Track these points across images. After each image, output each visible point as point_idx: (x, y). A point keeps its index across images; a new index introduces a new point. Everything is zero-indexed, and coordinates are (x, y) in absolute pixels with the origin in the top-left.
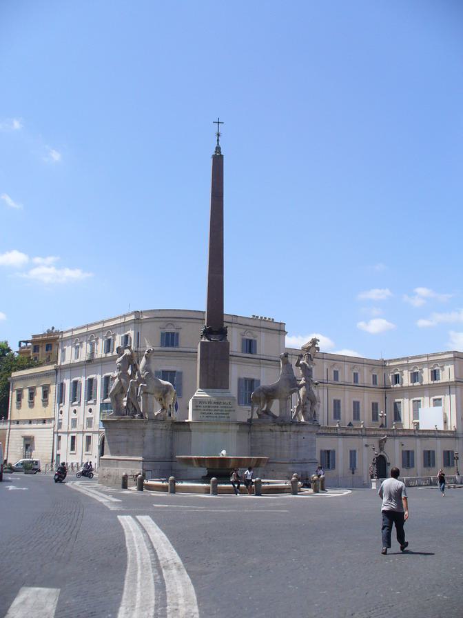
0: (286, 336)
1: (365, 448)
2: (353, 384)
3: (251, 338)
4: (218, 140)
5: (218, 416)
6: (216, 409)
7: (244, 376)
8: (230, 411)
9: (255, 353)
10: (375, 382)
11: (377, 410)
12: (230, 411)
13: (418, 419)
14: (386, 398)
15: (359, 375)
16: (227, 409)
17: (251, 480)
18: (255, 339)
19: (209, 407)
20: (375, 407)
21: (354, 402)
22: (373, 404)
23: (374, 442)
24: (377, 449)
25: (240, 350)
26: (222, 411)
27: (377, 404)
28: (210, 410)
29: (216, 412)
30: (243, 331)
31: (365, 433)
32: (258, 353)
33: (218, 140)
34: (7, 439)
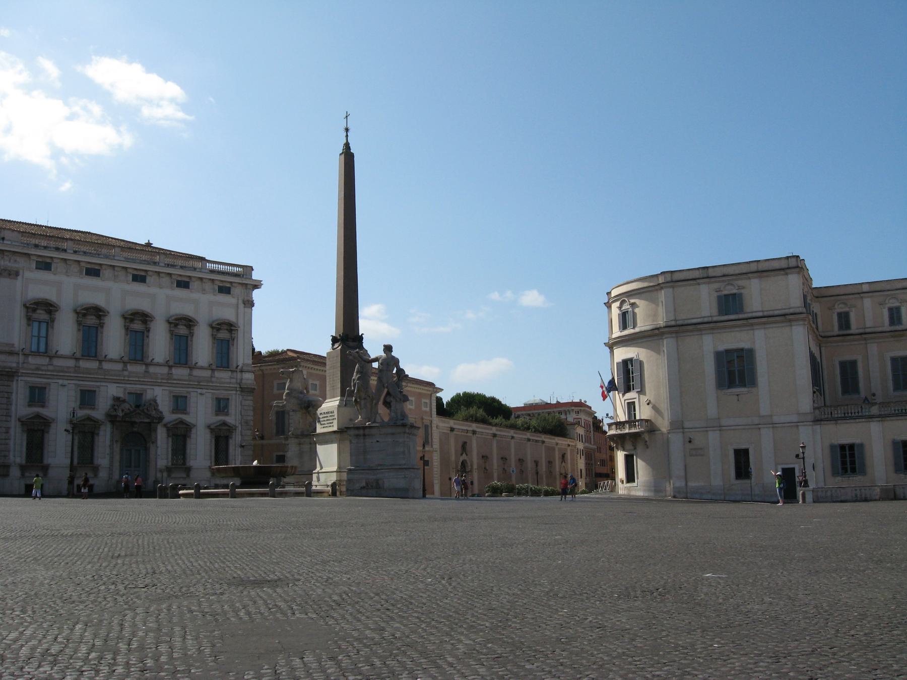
3: (735, 291)
4: (347, 136)
5: (328, 425)
7: (721, 348)
33: (347, 136)
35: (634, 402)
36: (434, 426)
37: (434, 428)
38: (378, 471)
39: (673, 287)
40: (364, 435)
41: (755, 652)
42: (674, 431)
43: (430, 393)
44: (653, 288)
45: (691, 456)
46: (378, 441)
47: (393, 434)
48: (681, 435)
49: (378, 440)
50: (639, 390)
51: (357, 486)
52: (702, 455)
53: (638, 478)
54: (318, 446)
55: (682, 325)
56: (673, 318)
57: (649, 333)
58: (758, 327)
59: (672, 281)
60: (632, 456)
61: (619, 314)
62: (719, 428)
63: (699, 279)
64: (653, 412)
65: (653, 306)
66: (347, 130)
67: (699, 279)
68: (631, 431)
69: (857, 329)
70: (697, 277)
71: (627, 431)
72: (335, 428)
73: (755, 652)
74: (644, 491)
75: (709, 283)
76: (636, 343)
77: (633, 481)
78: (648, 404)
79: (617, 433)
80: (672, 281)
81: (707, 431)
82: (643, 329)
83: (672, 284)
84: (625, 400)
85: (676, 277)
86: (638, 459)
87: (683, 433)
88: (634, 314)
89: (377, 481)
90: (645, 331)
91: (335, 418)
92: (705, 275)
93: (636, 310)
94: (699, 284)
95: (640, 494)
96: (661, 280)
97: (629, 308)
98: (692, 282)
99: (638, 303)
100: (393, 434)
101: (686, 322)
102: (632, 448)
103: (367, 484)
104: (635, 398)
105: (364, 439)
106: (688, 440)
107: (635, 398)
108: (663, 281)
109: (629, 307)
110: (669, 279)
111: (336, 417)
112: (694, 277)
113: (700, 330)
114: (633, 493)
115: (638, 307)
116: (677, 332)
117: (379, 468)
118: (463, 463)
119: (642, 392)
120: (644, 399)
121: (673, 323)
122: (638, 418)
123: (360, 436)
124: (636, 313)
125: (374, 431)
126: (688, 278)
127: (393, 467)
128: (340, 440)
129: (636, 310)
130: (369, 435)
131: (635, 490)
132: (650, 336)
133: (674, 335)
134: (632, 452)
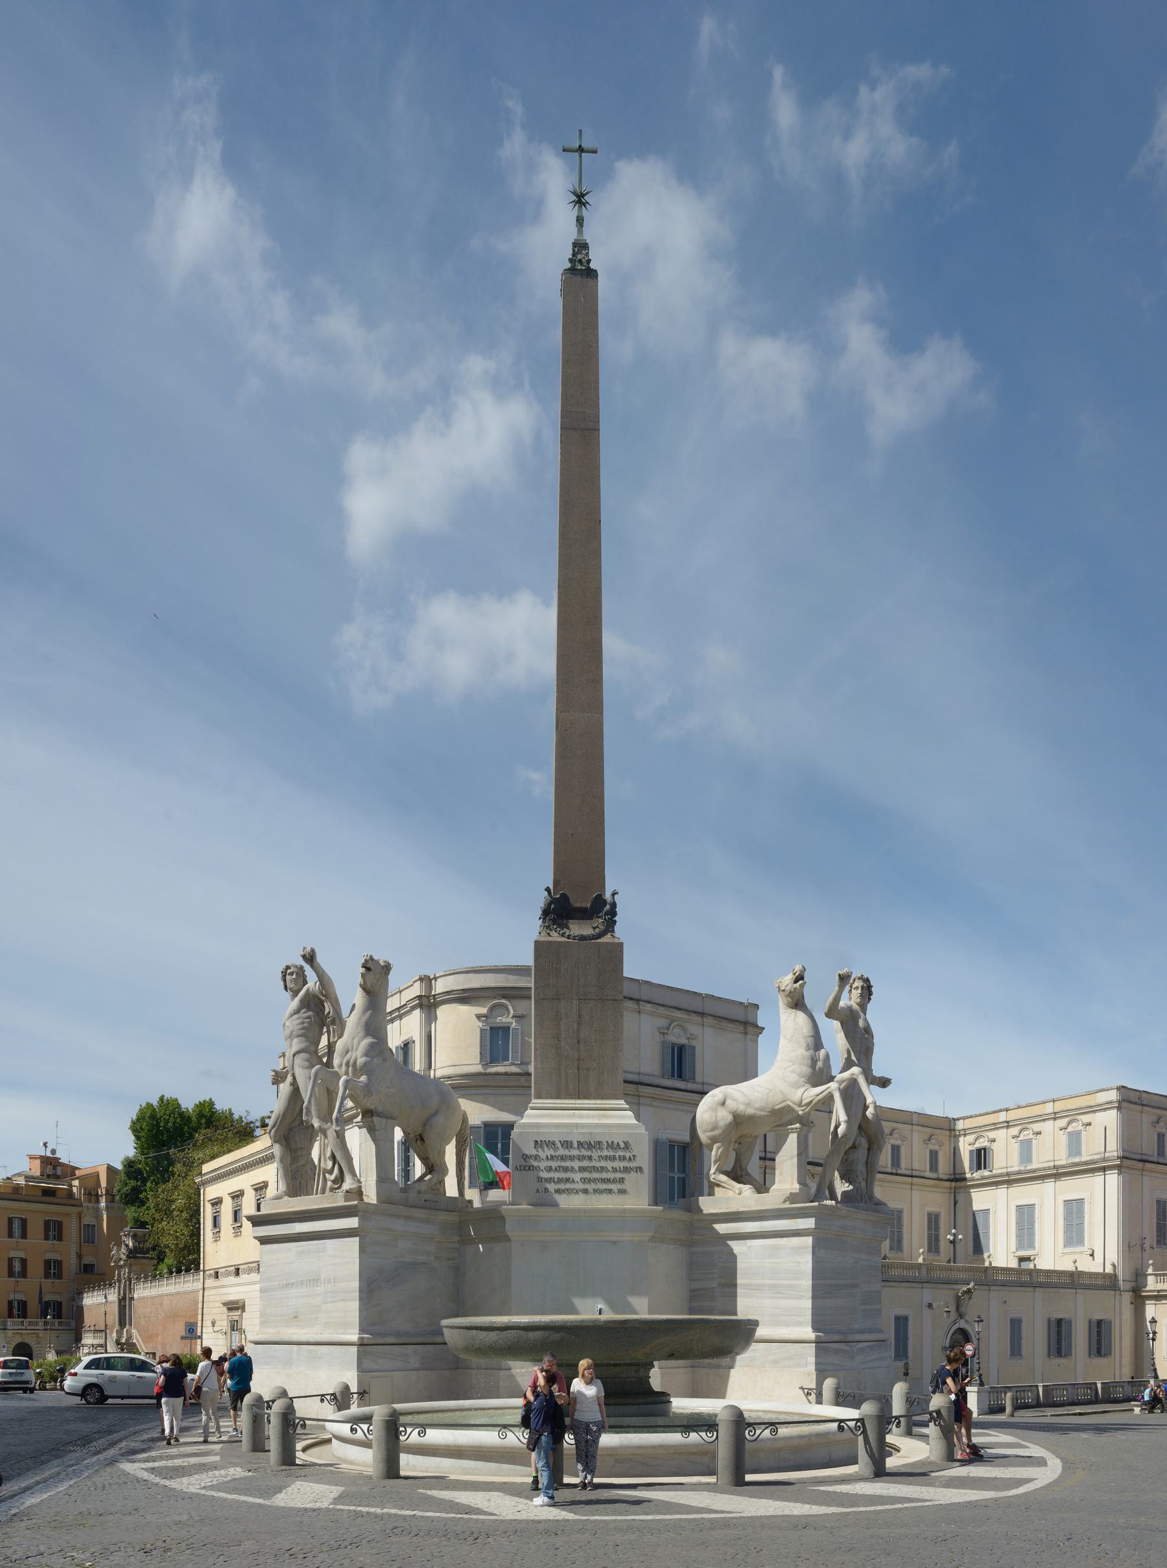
0: (761, 1038)
1: (926, 1311)
2: (889, 1170)
3: (683, 1041)
5: (591, 1187)
6: (585, 1163)
8: (626, 1170)
9: (693, 1079)
10: (934, 1166)
11: (937, 1228)
12: (626, 1170)
13: (1031, 1246)
14: (955, 1203)
15: (903, 1150)
16: (617, 1164)
17: (54, 1318)
18: (694, 1043)
19: (563, 1158)
20: (933, 1221)
21: (929, 1215)
22: (929, 1215)
23: (943, 1298)
24: (954, 1315)
25: (657, 1072)
26: (603, 1169)
27: (937, 1216)
28: (566, 1169)
29: (586, 1175)
30: (663, 1022)
31: (925, 1278)
32: (698, 1078)
33: (580, 221)
34: (200, 1311)
69: (905, 1169)
91: (639, 1169)
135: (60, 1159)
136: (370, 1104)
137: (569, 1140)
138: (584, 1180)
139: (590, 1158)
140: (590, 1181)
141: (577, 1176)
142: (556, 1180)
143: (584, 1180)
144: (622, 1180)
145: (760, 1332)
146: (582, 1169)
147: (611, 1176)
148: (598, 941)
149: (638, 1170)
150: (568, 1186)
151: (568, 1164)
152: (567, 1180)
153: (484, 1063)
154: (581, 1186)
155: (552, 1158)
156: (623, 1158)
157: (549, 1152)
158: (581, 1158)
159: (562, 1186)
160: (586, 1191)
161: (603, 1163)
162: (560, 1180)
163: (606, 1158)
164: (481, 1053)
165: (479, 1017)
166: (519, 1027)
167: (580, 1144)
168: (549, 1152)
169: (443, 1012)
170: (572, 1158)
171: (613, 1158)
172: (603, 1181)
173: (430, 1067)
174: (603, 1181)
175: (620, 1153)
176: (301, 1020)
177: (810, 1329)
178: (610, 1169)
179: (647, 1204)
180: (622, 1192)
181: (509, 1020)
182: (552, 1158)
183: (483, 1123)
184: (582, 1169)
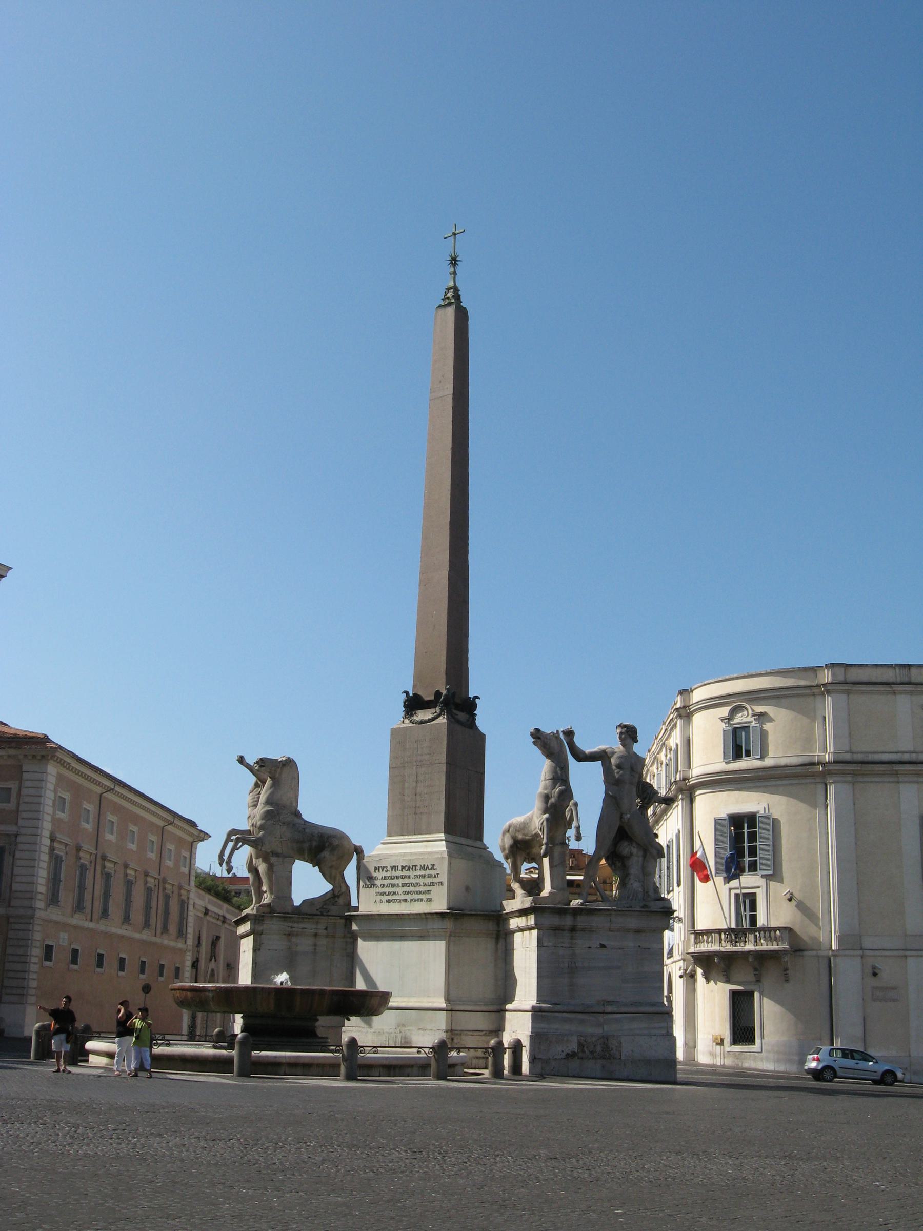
5: (408, 897)
6: (406, 881)
8: (432, 884)
12: (432, 884)
28: (393, 885)
29: (406, 889)
35: (755, 894)
36: (191, 902)
37: (191, 908)
38: (607, 1016)
39: (848, 692)
40: (573, 929)
41: (55, 1200)
42: (847, 952)
43: (190, 839)
44: (808, 691)
45: (874, 1000)
46: (603, 946)
47: (638, 931)
48: (859, 959)
49: (603, 943)
50: (771, 872)
51: (559, 1050)
52: (894, 1000)
53: (762, 1037)
54: (360, 942)
55: (863, 763)
56: (847, 749)
57: (799, 770)
58: (906, 779)
59: (846, 683)
60: (751, 994)
61: (724, 731)
62: (860, 952)
63: (894, 683)
64: (799, 915)
65: (806, 721)
66: (454, 261)
67: (894, 683)
68: (759, 948)
70: (891, 680)
71: (749, 947)
72: (440, 904)
73: (55, 1200)
74: (778, 1061)
75: (912, 693)
76: (765, 786)
77: (750, 1040)
78: (790, 900)
79: (722, 949)
80: (846, 683)
81: (906, 956)
82: (783, 761)
83: (846, 687)
84: (730, 889)
85: (853, 675)
86: (764, 998)
87: (862, 957)
88: (764, 735)
89: (605, 1038)
90: (786, 766)
91: (442, 883)
92: (906, 680)
93: (768, 726)
94: (894, 693)
95: (767, 1065)
96: (827, 677)
97: (751, 722)
98: (881, 688)
99: (772, 714)
100: (638, 931)
101: (871, 757)
102: (753, 979)
103: (581, 1045)
104: (759, 887)
105: (572, 938)
106: (870, 971)
107: (759, 887)
108: (830, 680)
109: (750, 719)
110: (841, 678)
111: (444, 878)
112: (884, 679)
113: (897, 774)
114: (749, 1064)
115: (771, 720)
116: (854, 774)
117: (609, 1009)
118: (213, 970)
119: (775, 875)
120: (780, 890)
121: (848, 757)
122: (761, 921)
123: (563, 930)
124: (767, 732)
125: (597, 921)
126: (874, 680)
127: (642, 1009)
128: (450, 936)
129: (768, 726)
130: (583, 930)
131: (755, 1059)
132: (796, 776)
133: (849, 778)
134: (750, 988)
135: (583, 851)
136: (267, 848)
137: (396, 865)
138: (406, 893)
139: (409, 877)
140: (408, 893)
141: (400, 890)
142: (387, 893)
143: (406, 893)
144: (429, 892)
145: (392, 1003)
146: (404, 885)
147: (422, 889)
148: (432, 723)
149: (440, 884)
150: (395, 897)
151: (395, 881)
152: (394, 893)
153: (727, 761)
154: (403, 897)
155: (385, 878)
156: (430, 876)
157: (384, 874)
158: (403, 877)
159: (390, 897)
160: (406, 900)
161: (418, 880)
162: (389, 894)
163: (420, 876)
164: (724, 752)
165: (722, 719)
166: (758, 725)
167: (403, 868)
168: (384, 874)
169: (698, 719)
170: (397, 877)
171: (423, 876)
172: (417, 893)
173: (689, 767)
174: (417, 893)
175: (428, 872)
176: (253, 797)
177: (443, 1000)
178: (422, 884)
179: (446, 908)
180: (429, 900)
181: (750, 719)
182: (385, 878)
183: (728, 815)
184: (404, 885)
